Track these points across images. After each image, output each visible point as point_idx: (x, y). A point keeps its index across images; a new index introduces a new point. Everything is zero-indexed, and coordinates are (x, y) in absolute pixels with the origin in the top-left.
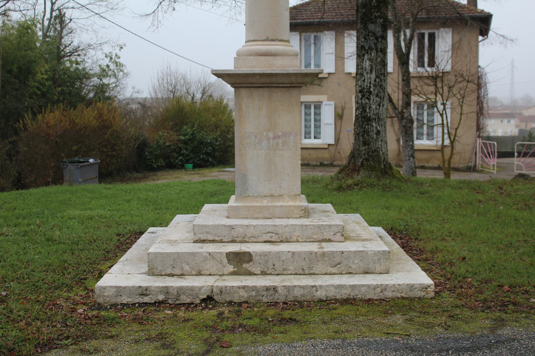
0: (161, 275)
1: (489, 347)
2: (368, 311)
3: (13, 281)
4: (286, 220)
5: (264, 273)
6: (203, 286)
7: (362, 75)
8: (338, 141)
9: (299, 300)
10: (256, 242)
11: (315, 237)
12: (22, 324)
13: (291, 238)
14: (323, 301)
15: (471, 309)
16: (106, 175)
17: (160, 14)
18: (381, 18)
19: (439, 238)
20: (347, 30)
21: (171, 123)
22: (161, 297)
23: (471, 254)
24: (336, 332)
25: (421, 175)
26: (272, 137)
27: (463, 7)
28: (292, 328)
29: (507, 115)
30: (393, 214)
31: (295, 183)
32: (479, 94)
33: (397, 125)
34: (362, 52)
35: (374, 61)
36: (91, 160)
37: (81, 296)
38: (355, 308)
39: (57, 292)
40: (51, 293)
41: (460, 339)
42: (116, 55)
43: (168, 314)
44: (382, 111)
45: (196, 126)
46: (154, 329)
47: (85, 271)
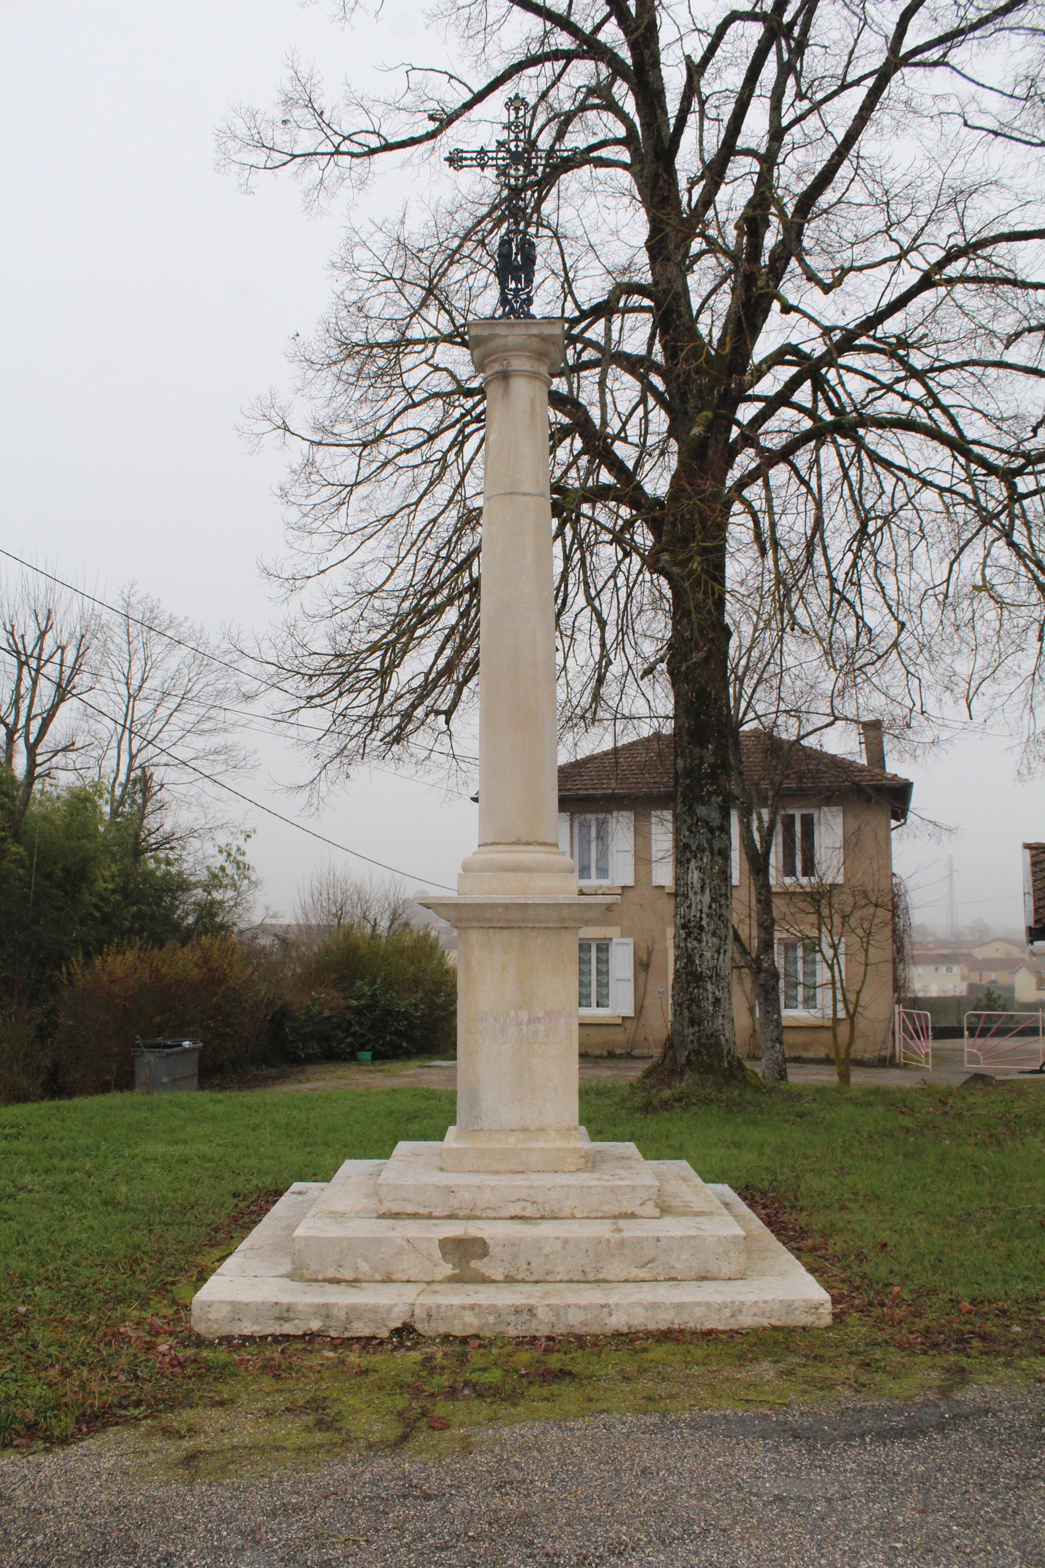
0: (317, 1281)
1: (941, 1427)
2: (708, 1355)
3: (39, 1283)
4: (551, 1175)
5: (509, 1280)
6: (396, 1305)
7: (686, 896)
8: (641, 1012)
9: (577, 1332)
10: (495, 1218)
11: (606, 1208)
12: (53, 1372)
13: (560, 1210)
14: (622, 1335)
15: (901, 1347)
16: (214, 1072)
17: (323, 786)
18: (718, 795)
19: (836, 1206)
20: (656, 809)
21: (333, 976)
22: (315, 1325)
23: (896, 1237)
24: (649, 1399)
25: (798, 1077)
26: (525, 1020)
27: (862, 769)
28: (567, 1391)
29: (946, 957)
30: (748, 1157)
31: (566, 1106)
32: (895, 924)
33: (748, 982)
34: (683, 854)
35: (708, 872)
36: (186, 1044)
37: (165, 1317)
38: (682, 1348)
39: (121, 1309)
40: (109, 1310)
41: (885, 1412)
42: (239, 850)
43: (328, 1358)
44: (725, 964)
45: (379, 981)
46: (301, 1390)
47: (173, 1267)
